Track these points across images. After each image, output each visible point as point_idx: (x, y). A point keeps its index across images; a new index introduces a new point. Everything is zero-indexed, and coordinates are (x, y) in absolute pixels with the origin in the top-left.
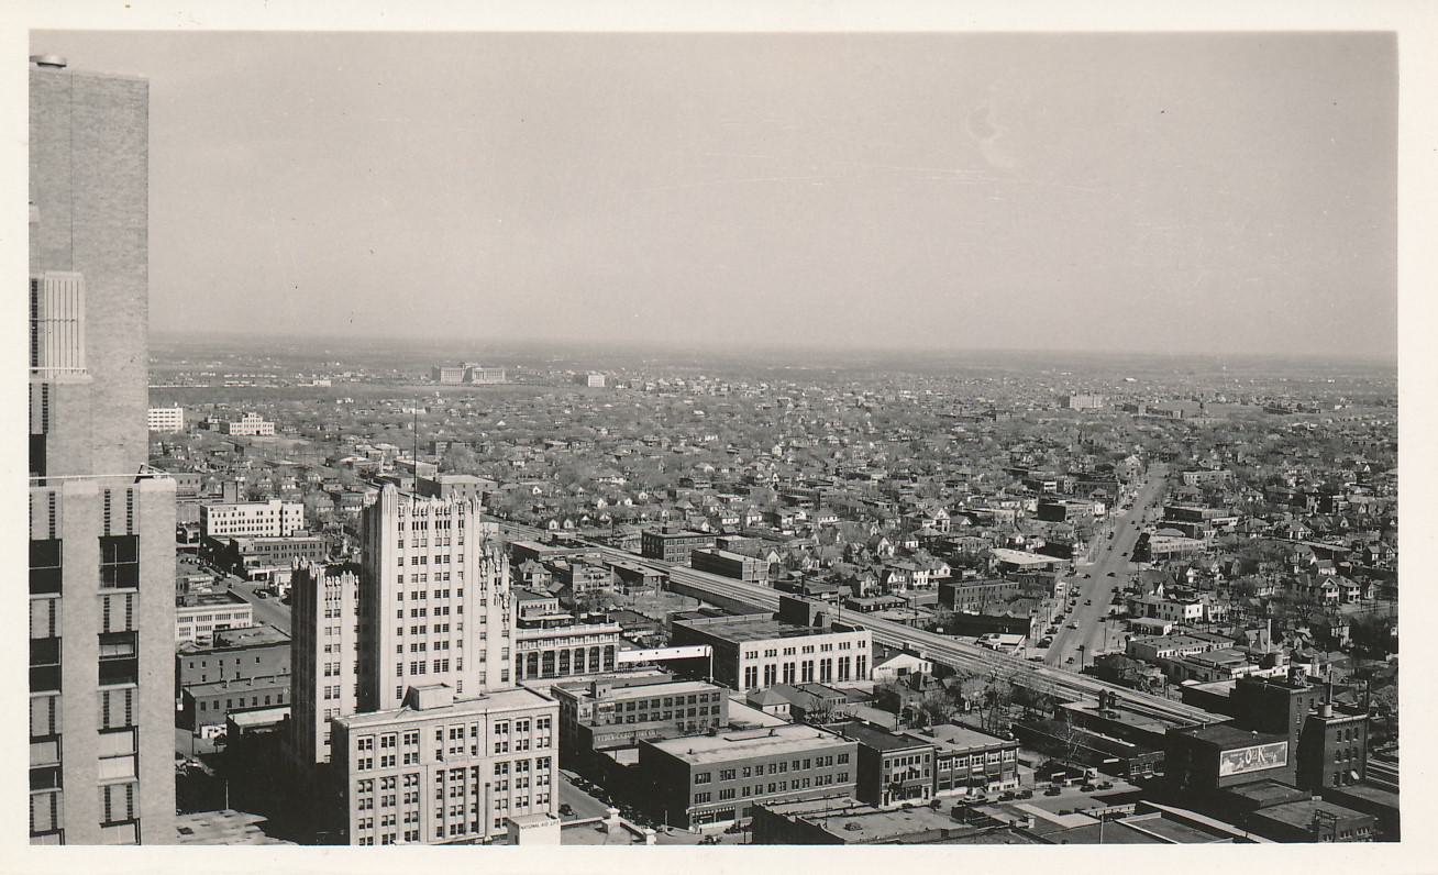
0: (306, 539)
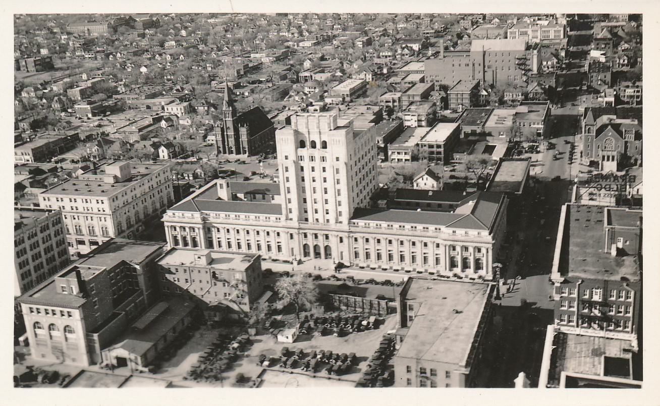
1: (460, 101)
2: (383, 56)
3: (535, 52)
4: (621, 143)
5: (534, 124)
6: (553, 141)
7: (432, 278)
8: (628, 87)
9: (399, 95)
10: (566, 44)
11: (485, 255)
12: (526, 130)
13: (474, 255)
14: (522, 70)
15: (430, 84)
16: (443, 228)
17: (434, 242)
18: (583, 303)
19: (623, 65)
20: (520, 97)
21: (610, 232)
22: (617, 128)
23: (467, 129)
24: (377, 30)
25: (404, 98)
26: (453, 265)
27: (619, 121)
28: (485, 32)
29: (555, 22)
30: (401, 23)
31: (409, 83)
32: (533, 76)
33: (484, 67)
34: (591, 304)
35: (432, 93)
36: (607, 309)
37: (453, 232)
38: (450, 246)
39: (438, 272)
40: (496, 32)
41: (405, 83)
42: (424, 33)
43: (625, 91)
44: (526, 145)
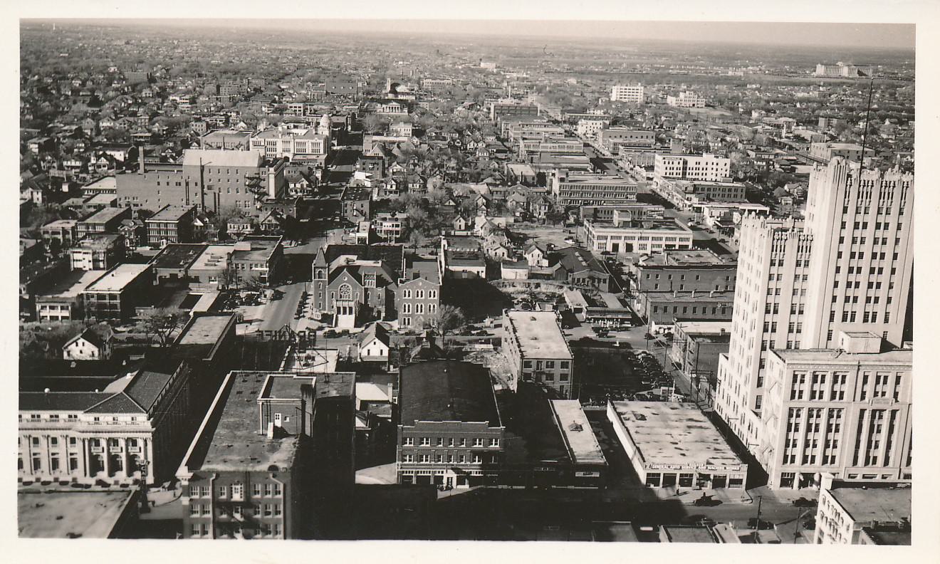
0: (731, 185)
1: (163, 234)
2: (68, 167)
3: (272, 170)
4: (360, 293)
5: (256, 266)
6: (282, 289)
7: (48, 489)
8: (385, 219)
9: (73, 223)
10: (323, 162)
11: (142, 450)
12: (245, 275)
13: (127, 449)
14: (255, 193)
15: (124, 208)
16: (80, 414)
17: (30, 436)
18: (217, 504)
19: (391, 192)
20: (249, 229)
21: (265, 409)
22: (354, 270)
23: (165, 273)
24: (66, 128)
25: (81, 228)
26: (95, 466)
27: (358, 263)
28: (220, 140)
29: (314, 132)
30: (105, 120)
31: (95, 207)
32: (269, 202)
33: (203, 187)
34: (230, 506)
35: (124, 222)
36: (251, 511)
37: (95, 419)
38: (90, 440)
39: (74, 480)
40: (237, 141)
41: (89, 207)
42: (136, 137)
43: (381, 224)
44: (243, 294)
